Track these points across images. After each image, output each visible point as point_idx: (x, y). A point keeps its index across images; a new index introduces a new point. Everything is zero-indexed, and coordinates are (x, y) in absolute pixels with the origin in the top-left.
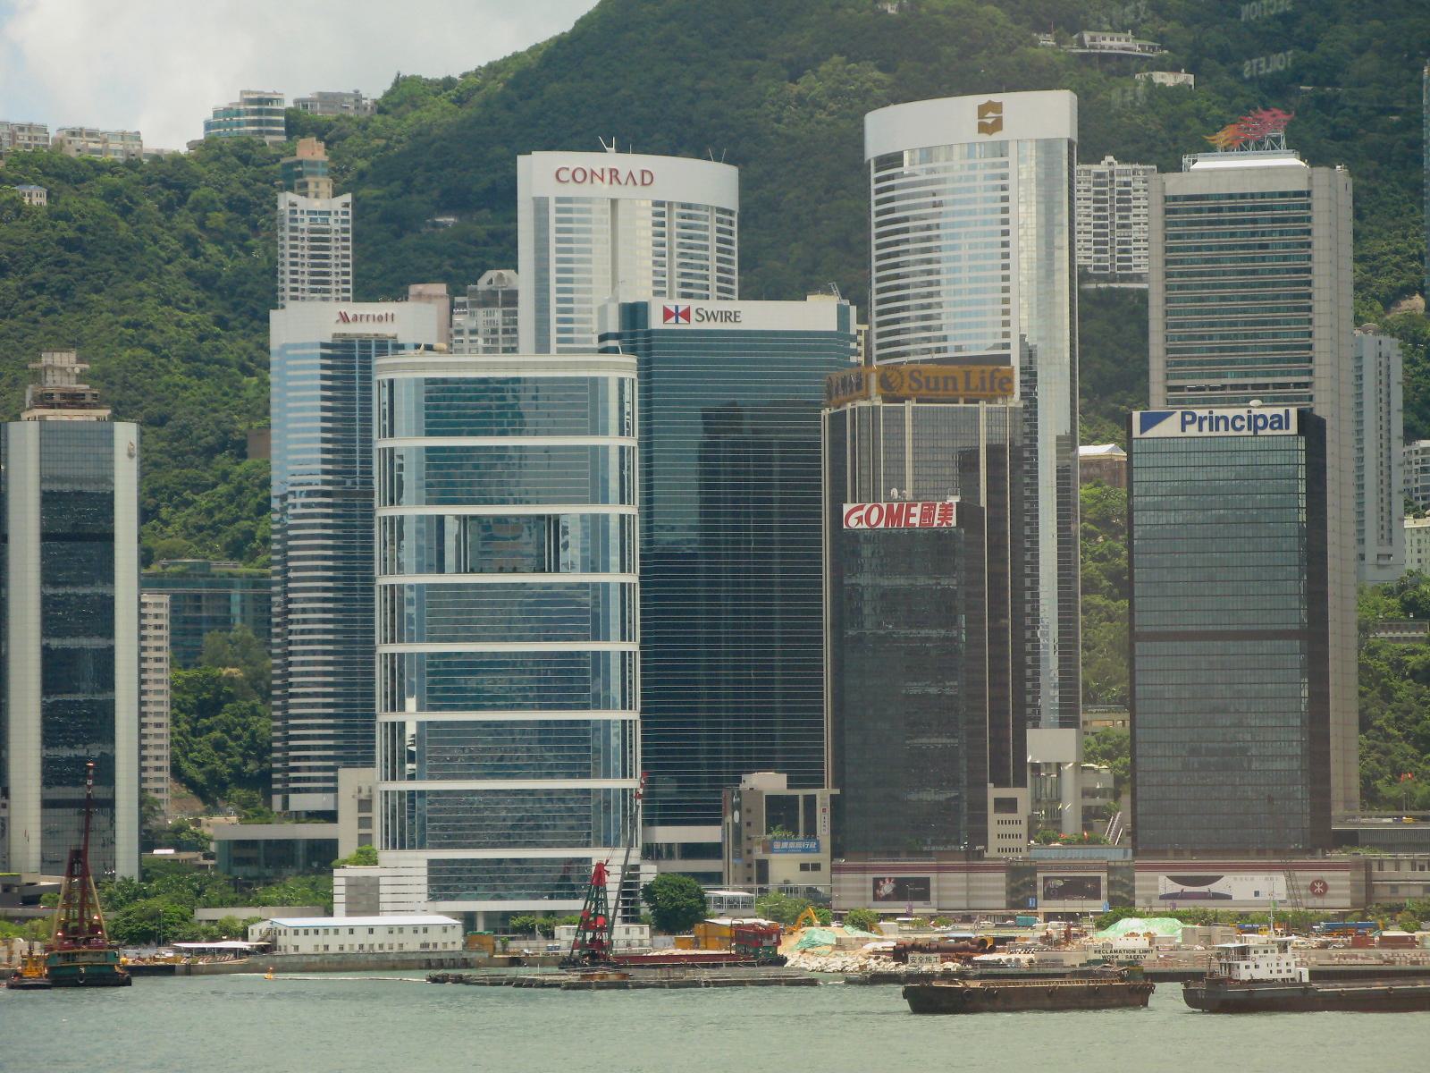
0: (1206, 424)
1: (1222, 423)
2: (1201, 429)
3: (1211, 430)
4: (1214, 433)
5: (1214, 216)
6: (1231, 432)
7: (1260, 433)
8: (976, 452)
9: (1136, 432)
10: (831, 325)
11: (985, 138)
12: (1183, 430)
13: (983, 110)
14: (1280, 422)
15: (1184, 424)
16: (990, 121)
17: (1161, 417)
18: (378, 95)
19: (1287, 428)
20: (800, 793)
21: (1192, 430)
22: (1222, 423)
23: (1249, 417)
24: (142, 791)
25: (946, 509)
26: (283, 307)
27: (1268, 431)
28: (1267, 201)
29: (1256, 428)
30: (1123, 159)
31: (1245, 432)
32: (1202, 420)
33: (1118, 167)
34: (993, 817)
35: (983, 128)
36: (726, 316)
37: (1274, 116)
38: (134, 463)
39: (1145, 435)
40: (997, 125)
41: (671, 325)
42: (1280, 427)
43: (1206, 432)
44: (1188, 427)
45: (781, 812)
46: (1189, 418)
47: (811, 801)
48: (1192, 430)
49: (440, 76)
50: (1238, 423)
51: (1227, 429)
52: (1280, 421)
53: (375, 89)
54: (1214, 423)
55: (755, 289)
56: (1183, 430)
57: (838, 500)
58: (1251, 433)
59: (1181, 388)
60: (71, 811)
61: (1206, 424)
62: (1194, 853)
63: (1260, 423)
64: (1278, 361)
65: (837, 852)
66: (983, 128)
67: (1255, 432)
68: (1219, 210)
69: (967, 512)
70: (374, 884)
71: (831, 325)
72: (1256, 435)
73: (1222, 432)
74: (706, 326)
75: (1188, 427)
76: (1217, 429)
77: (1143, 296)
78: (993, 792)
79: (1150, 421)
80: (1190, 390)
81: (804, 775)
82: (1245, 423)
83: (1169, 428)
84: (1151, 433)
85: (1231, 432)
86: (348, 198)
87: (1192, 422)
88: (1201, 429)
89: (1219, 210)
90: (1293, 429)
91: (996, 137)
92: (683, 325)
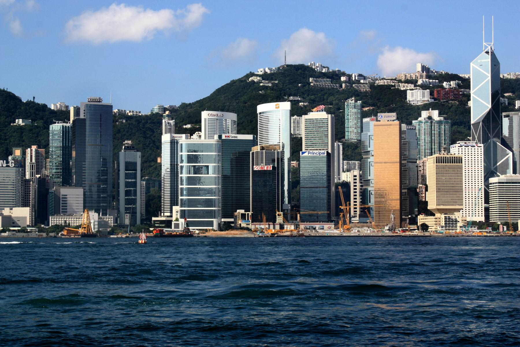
8: (275, 159)
9: (301, 155)
10: (252, 139)
11: (276, 109)
13: (276, 105)
14: (323, 153)
17: (304, 153)
18: (179, 106)
20: (247, 213)
21: (310, 155)
24: (141, 213)
25: (270, 167)
28: (322, 120)
30: (297, 116)
33: (297, 117)
34: (277, 217)
35: (276, 108)
36: (235, 137)
38: (140, 159)
40: (278, 107)
41: (226, 138)
43: (312, 155)
45: (243, 216)
47: (248, 214)
48: (310, 155)
49: (189, 103)
54: (313, 153)
55: (239, 132)
57: (253, 165)
62: (309, 222)
65: (252, 222)
66: (276, 108)
69: (274, 167)
70: (178, 224)
71: (252, 139)
74: (232, 138)
77: (301, 138)
78: (277, 213)
79: (303, 153)
81: (247, 210)
83: (306, 154)
84: (303, 155)
86: (174, 120)
90: (326, 155)
91: (278, 109)
92: (228, 138)
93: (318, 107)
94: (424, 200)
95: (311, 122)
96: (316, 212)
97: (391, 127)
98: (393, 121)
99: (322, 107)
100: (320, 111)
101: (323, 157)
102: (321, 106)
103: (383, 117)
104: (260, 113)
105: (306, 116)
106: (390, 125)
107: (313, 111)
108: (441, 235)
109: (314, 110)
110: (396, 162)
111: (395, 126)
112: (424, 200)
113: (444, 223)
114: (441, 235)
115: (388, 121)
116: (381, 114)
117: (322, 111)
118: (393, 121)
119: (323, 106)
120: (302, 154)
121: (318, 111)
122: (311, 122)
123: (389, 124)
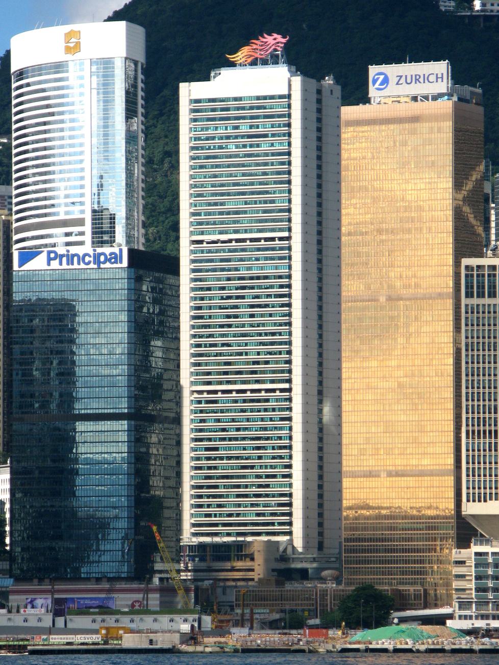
0: (64, 259)
1: (76, 259)
2: (61, 264)
3: (68, 264)
4: (70, 267)
5: (224, 114)
6: (82, 266)
7: (102, 266)
9: (16, 266)
11: (69, 57)
12: (49, 264)
13: (69, 36)
15: (49, 260)
16: (72, 45)
19: (121, 262)
21: (55, 264)
22: (76, 259)
23: (94, 255)
26: (114, 214)
27: (108, 265)
29: (99, 263)
31: (92, 266)
32: (62, 256)
35: (68, 50)
37: (275, 39)
39: (22, 268)
42: (116, 262)
43: (65, 266)
44: (52, 262)
46: (52, 255)
48: (55, 264)
50: (87, 259)
51: (79, 264)
52: (116, 258)
53: (361, 105)
56: (49, 264)
58: (96, 266)
59: (201, 242)
60: (452, 505)
61: (64, 259)
63: (102, 258)
64: (266, 221)
67: (99, 265)
68: (227, 109)
72: (99, 268)
73: (76, 266)
75: (52, 262)
76: (72, 264)
80: (208, 243)
82: (92, 259)
84: (26, 267)
85: (82, 266)
87: (55, 259)
88: (61, 264)
89: (227, 109)
90: (125, 263)
93: (257, 44)
94: (126, 454)
95: (218, 114)
96: (238, 636)
97: (424, 127)
98: (435, 98)
99: (274, 41)
100: (265, 62)
101: (449, 293)
102: (269, 39)
103: (393, 80)
104: (21, 74)
105: (195, 85)
106: (415, 119)
107: (232, 65)
108: (119, 646)
109: (241, 55)
110: (440, 296)
111: (435, 125)
112: (126, 454)
113: (289, 589)
114: (119, 646)
115: (415, 99)
116: (383, 68)
117: (274, 60)
118: (435, 98)
119: (279, 38)
120: (21, 265)
121: (254, 63)
122: (218, 114)
123: (410, 114)
